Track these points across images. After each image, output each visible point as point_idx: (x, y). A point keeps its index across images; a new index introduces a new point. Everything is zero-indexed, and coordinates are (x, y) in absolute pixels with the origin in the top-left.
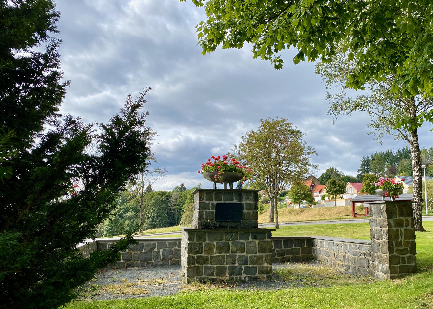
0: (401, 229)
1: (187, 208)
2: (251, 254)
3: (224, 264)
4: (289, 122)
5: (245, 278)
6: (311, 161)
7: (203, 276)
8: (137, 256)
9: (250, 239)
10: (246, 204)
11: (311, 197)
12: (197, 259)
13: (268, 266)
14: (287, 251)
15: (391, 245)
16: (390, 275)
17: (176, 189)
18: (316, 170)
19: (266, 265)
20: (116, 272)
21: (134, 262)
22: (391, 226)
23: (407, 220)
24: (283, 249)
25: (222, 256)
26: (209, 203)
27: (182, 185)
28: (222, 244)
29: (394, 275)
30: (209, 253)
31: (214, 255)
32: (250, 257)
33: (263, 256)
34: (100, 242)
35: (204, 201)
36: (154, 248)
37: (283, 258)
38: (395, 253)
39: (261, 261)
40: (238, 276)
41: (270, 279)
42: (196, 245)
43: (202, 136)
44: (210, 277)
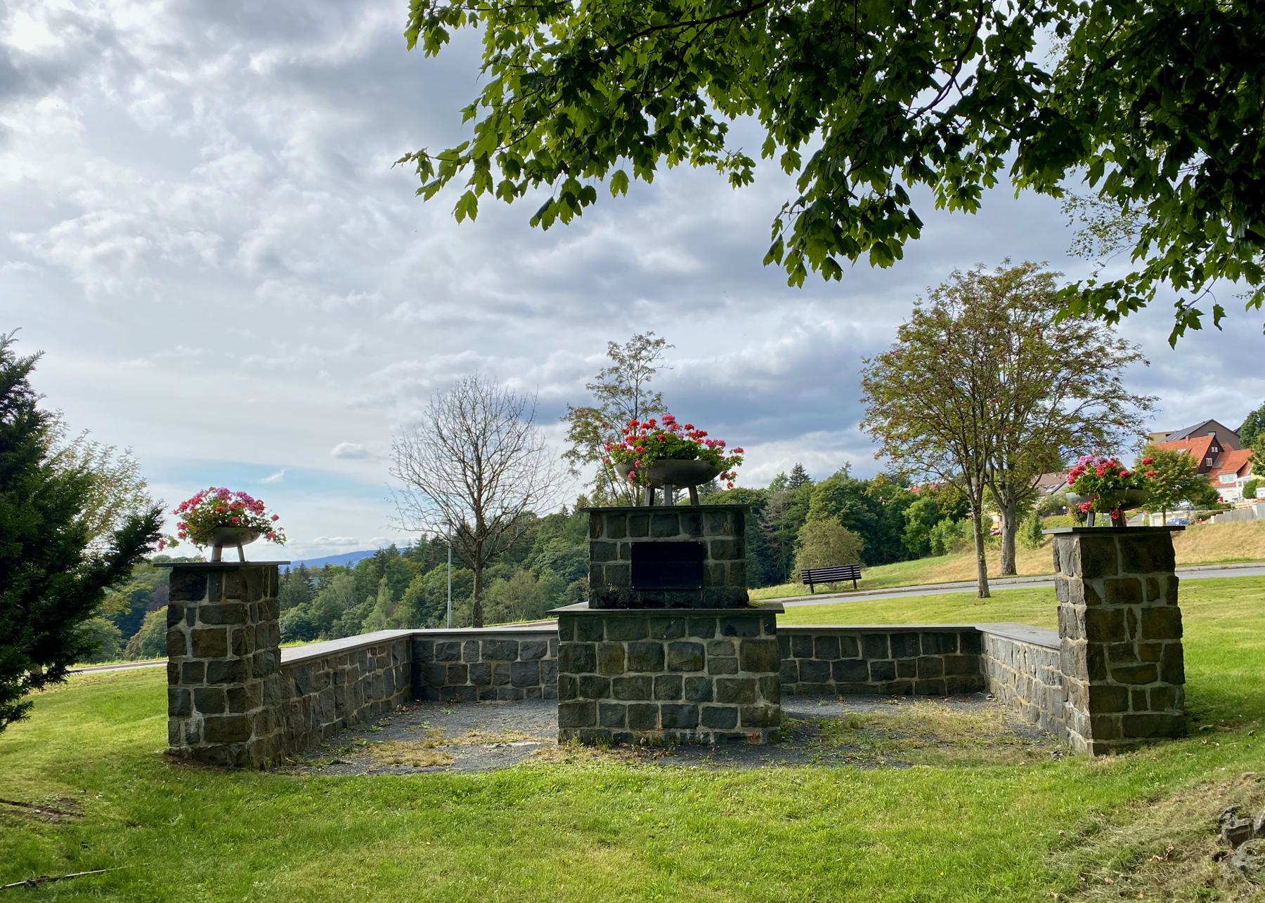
0: (1130, 611)
1: (809, 535)
2: (720, 673)
3: (649, 699)
4: (1051, 271)
5: (707, 735)
6: (1128, 389)
7: (596, 728)
8: (504, 672)
9: (718, 636)
10: (713, 543)
11: (1203, 489)
12: (582, 684)
13: (768, 708)
14: (901, 665)
15: (1096, 654)
16: (1092, 741)
17: (777, 481)
18: (1148, 412)
19: (761, 703)
20: (444, 710)
21: (498, 688)
22: (1099, 601)
23: (1153, 583)
24: (890, 659)
25: (643, 678)
26: (615, 544)
27: (799, 470)
28: (643, 649)
29: (1105, 742)
30: (609, 672)
31: (625, 675)
32: (718, 681)
33: (753, 680)
34: (419, 639)
35: (604, 538)
36: (544, 653)
37: (890, 686)
38: (1110, 679)
39: (748, 693)
40: (688, 731)
41: (777, 739)
42: (579, 650)
43: (856, 324)
44: (616, 731)
